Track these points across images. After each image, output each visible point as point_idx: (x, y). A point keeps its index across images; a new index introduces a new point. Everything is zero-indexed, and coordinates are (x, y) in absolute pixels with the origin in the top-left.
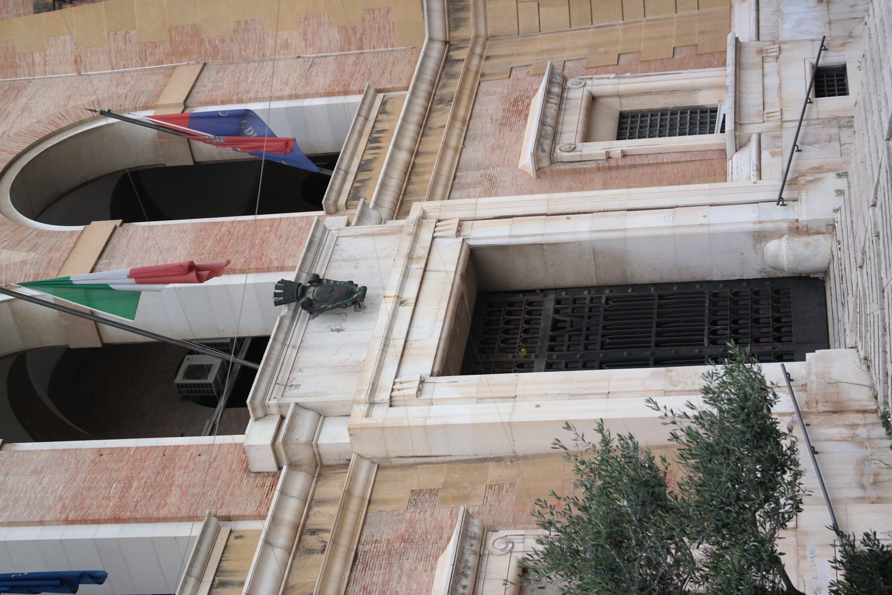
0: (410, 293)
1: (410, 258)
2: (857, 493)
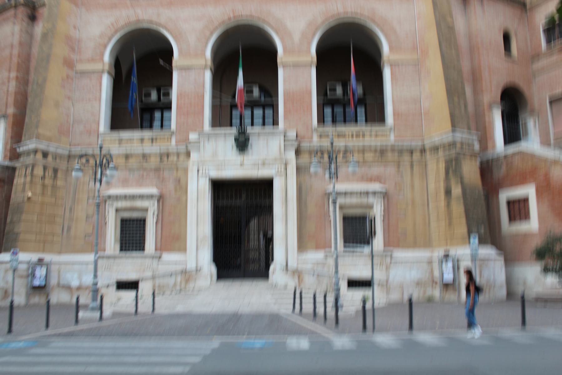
2: (157, 285)
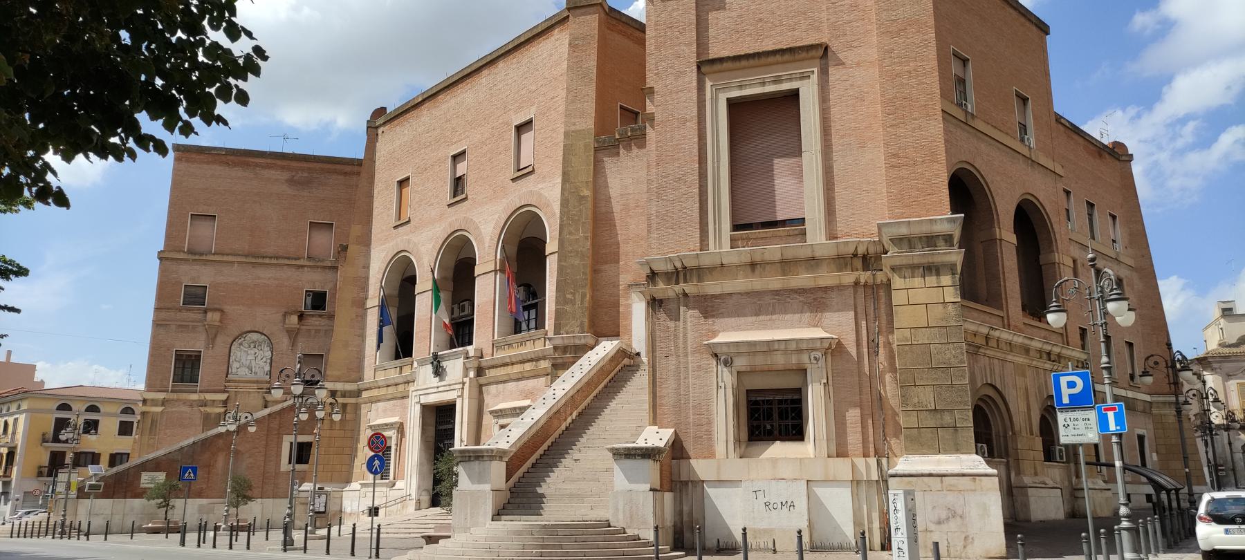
0: (440, 389)
1: (450, 385)
